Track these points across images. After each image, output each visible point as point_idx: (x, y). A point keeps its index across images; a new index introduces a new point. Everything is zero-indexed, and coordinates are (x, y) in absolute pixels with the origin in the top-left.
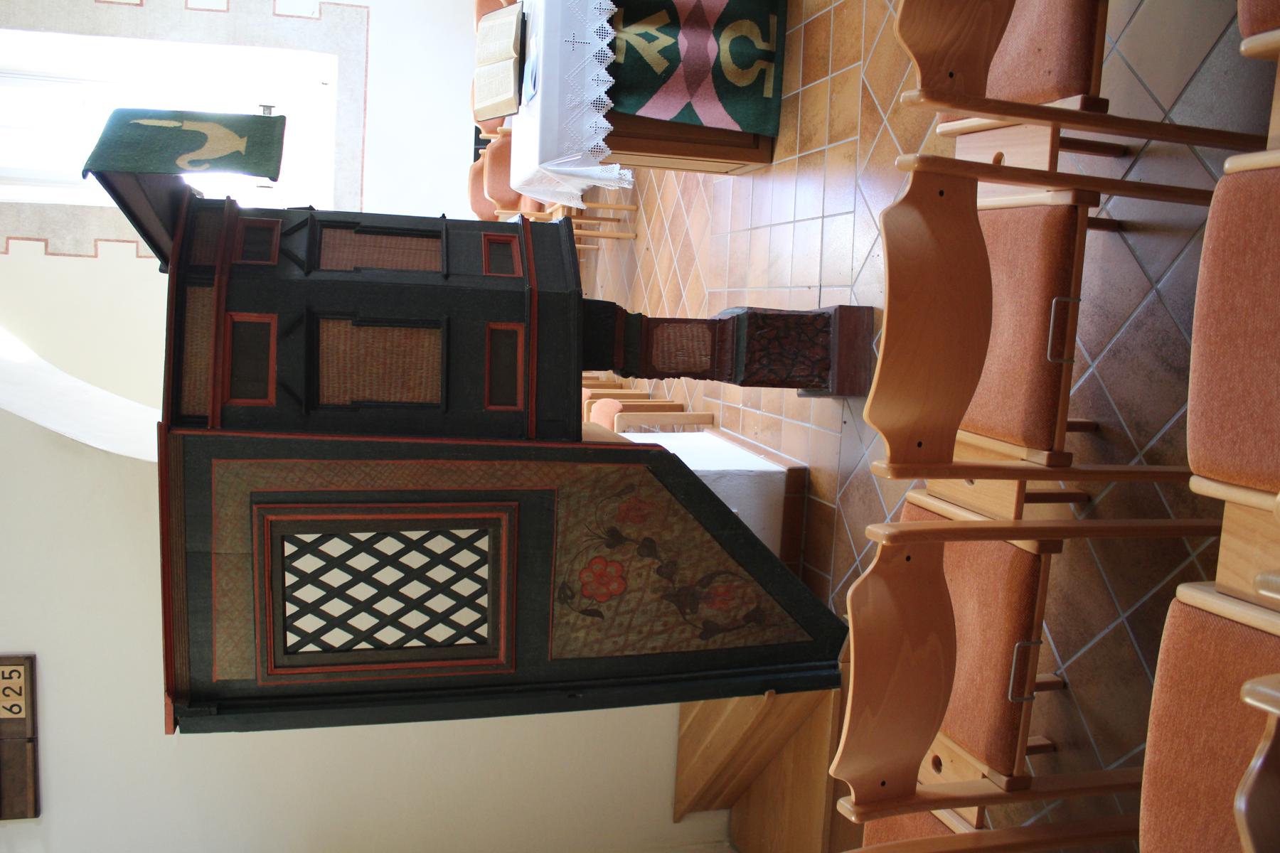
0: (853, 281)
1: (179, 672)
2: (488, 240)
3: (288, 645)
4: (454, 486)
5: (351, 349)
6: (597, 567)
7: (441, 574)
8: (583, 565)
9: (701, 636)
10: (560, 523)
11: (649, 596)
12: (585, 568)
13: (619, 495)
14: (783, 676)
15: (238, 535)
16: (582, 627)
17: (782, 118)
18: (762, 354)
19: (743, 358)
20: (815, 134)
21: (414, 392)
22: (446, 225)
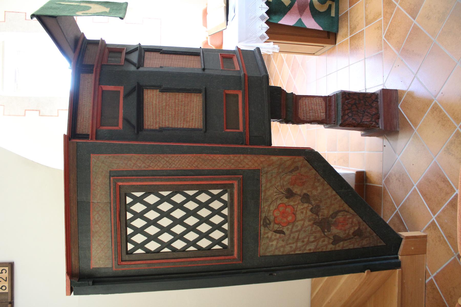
0: (384, 81)
1: (74, 263)
2: (222, 56)
3: (128, 249)
4: (211, 168)
5: (159, 103)
6: (281, 209)
7: (204, 213)
8: (274, 207)
9: (332, 243)
10: (263, 186)
11: (307, 223)
12: (275, 209)
13: (291, 172)
14: (371, 263)
15: (103, 193)
16: (275, 239)
17: (340, 25)
18: (349, 111)
19: (340, 114)
20: (358, 25)
21: (189, 123)
22: (202, 50)
